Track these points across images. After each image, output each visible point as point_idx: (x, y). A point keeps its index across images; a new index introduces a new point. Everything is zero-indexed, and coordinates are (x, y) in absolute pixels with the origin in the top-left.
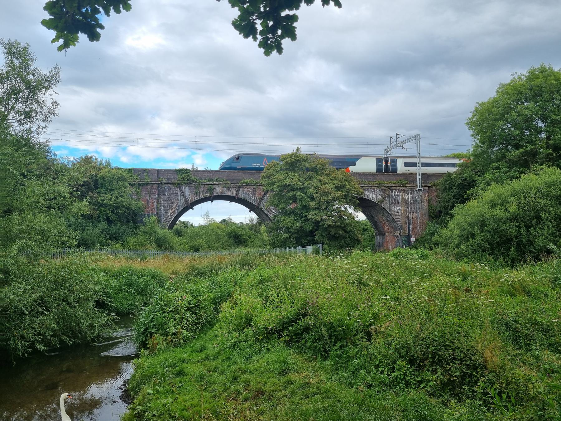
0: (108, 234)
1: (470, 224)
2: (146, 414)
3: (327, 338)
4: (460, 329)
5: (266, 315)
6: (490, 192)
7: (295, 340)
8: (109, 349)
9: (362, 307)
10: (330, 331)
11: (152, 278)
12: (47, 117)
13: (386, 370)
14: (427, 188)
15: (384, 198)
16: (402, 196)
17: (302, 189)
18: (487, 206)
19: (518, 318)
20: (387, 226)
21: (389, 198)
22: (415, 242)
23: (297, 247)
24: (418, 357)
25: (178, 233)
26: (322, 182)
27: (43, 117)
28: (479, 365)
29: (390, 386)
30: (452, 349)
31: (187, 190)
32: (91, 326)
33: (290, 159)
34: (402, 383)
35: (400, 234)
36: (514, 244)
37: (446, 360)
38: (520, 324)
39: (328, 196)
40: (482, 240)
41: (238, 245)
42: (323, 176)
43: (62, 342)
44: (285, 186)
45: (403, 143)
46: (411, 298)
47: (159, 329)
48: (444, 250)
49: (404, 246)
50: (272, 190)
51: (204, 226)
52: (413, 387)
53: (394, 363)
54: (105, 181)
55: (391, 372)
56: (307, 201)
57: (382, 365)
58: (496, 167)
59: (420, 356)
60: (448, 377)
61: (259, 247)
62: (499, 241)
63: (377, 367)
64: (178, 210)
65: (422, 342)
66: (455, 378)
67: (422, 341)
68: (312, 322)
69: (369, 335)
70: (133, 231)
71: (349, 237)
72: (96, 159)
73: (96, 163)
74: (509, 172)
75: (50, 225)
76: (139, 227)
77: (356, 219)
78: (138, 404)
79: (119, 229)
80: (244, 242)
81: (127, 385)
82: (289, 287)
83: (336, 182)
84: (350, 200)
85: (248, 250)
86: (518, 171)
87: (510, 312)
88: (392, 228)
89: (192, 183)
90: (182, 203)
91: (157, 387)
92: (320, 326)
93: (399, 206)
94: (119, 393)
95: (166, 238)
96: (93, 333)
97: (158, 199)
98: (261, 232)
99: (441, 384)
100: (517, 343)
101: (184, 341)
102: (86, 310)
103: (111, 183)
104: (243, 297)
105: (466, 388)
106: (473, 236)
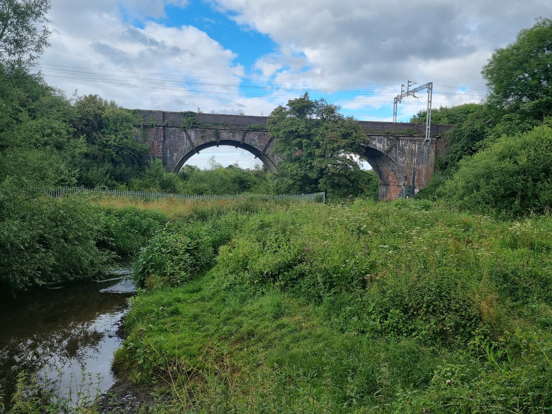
0: (113, 175)
1: (476, 177)
2: (138, 350)
3: (321, 284)
4: (458, 280)
5: (262, 260)
6: (499, 143)
7: (290, 285)
8: (110, 286)
9: (359, 255)
10: (325, 278)
11: (155, 219)
12: (39, 46)
13: (379, 317)
14: (436, 139)
15: (391, 148)
16: (409, 146)
18: (495, 158)
19: (517, 271)
20: (392, 176)
21: (396, 148)
22: (418, 193)
23: (301, 194)
24: (412, 306)
25: (184, 177)
26: (329, 130)
27: (34, 46)
28: (475, 316)
29: (381, 333)
30: (448, 300)
31: (192, 134)
32: (92, 263)
33: (297, 105)
35: (404, 185)
36: (518, 198)
37: (441, 310)
38: (518, 277)
39: (333, 144)
40: (487, 192)
41: (243, 191)
42: (330, 123)
43: (64, 277)
44: (291, 132)
46: (410, 247)
47: (157, 269)
48: (447, 201)
49: (408, 197)
50: (278, 137)
51: (209, 171)
52: (405, 335)
53: (388, 310)
54: (109, 121)
55: (383, 320)
56: (313, 148)
57: (375, 313)
58: (508, 119)
59: (415, 306)
60: (441, 327)
62: (504, 193)
63: (370, 314)
64: (184, 154)
65: (417, 292)
66: (448, 328)
67: (418, 290)
68: (307, 268)
69: (364, 284)
70: (138, 173)
71: (352, 186)
72: (101, 99)
73: (101, 103)
74: (522, 123)
75: (45, 163)
76: (144, 170)
77: (361, 169)
78: (131, 340)
79: (124, 171)
80: (249, 188)
81: (123, 321)
82: (288, 233)
83: (342, 129)
84: (356, 149)
85: (252, 195)
86: (531, 123)
87: (510, 264)
88: (397, 178)
89: (197, 127)
90: (187, 146)
91: (151, 325)
92: (315, 272)
93: (405, 157)
94: (116, 328)
95: (171, 181)
96: (94, 270)
97: (164, 142)
98: (267, 178)
99: (434, 333)
100: (514, 295)
101: (181, 282)
102: (87, 248)
103: (115, 123)
104: (241, 241)
105: (459, 338)
106: (478, 188)
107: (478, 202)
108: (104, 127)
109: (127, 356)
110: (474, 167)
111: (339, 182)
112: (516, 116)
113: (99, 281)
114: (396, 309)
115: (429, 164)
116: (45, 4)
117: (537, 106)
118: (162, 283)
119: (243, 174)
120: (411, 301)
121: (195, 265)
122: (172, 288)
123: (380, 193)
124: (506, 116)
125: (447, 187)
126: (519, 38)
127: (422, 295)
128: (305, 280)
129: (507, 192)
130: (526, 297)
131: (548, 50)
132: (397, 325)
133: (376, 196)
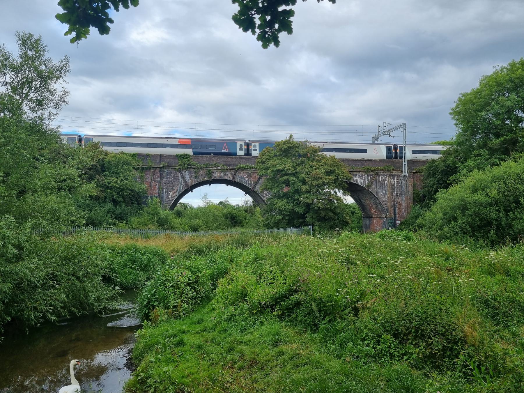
0: (114, 214)
1: (453, 208)
2: (149, 380)
4: (442, 306)
5: (260, 291)
6: (471, 178)
7: (287, 314)
10: (319, 307)
12: (58, 104)
13: (372, 343)
14: (413, 174)
15: (372, 183)
17: (295, 174)
18: (469, 191)
19: (496, 297)
20: (374, 209)
21: (376, 184)
22: (400, 224)
23: (290, 228)
24: (402, 331)
25: (179, 214)
26: (314, 168)
28: (460, 339)
29: (375, 358)
30: (434, 324)
31: (187, 174)
32: (98, 299)
33: (283, 146)
34: (387, 356)
38: (498, 302)
40: (464, 223)
41: (235, 225)
43: (71, 313)
44: (279, 171)
45: (390, 131)
46: (396, 276)
49: (390, 228)
50: (266, 175)
52: (397, 359)
54: (111, 165)
55: (376, 345)
57: (368, 338)
58: (478, 155)
61: (254, 228)
62: (480, 224)
63: (363, 340)
66: (436, 352)
67: (406, 316)
68: (303, 297)
69: (356, 311)
70: (137, 212)
74: (490, 159)
76: (142, 208)
81: (131, 354)
82: (282, 265)
83: (326, 167)
84: (340, 185)
85: (243, 230)
88: (379, 211)
89: (192, 168)
90: (182, 186)
91: (159, 356)
93: (385, 191)
94: (124, 361)
95: (167, 219)
97: (160, 182)
98: (256, 213)
100: (495, 320)
103: (117, 167)
104: (239, 274)
106: (455, 219)
107: (457, 232)
108: (106, 170)
109: (138, 386)
110: (450, 200)
111: (325, 216)
112: (485, 152)
113: (104, 316)
114: (387, 335)
115: (408, 197)
116: (64, 69)
117: (503, 143)
118: (166, 316)
119: (234, 210)
120: (401, 326)
121: (195, 297)
122: (176, 321)
123: (363, 225)
124: (476, 152)
125: (427, 218)
126: (480, 83)
127: (410, 320)
128: (301, 309)
129: (483, 223)
130: (507, 321)
131: (508, 93)
132: (389, 350)
133: (360, 228)
